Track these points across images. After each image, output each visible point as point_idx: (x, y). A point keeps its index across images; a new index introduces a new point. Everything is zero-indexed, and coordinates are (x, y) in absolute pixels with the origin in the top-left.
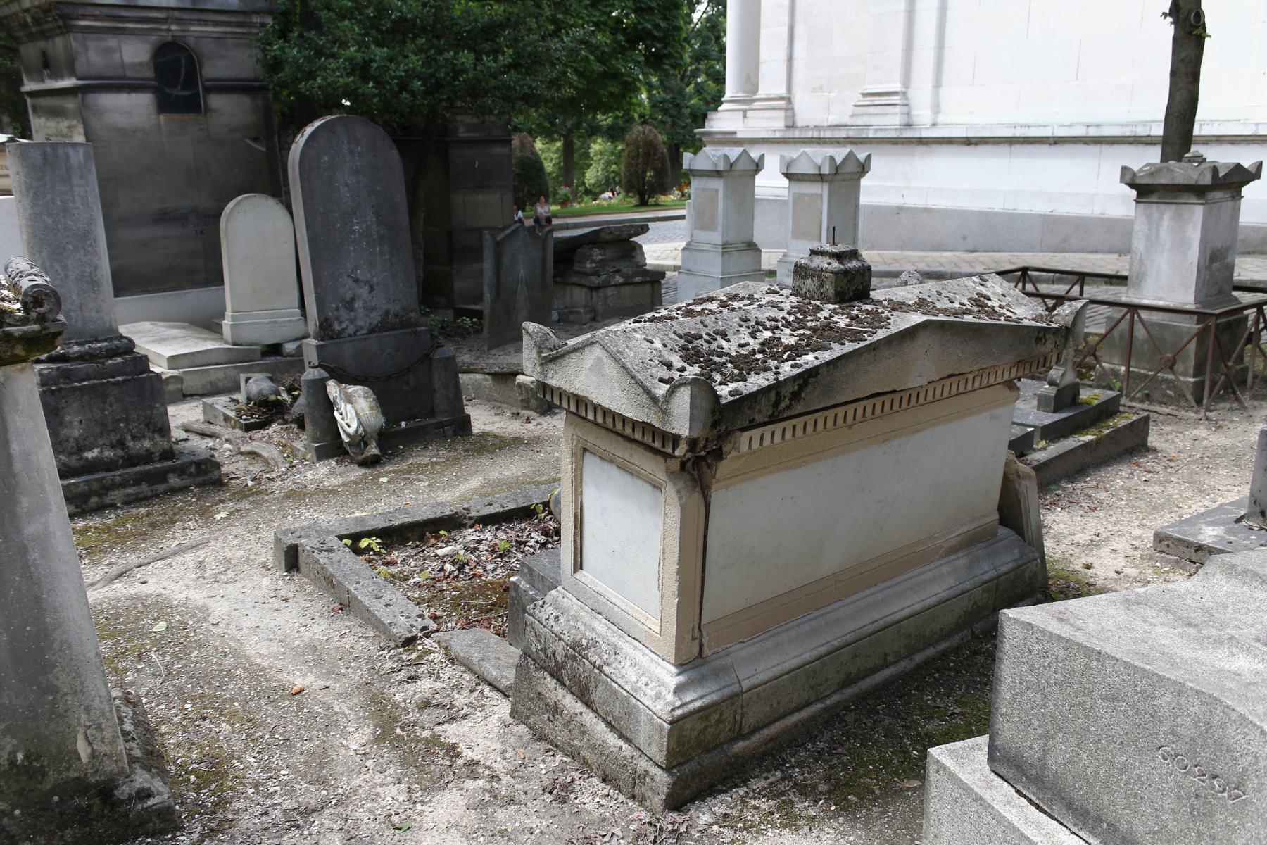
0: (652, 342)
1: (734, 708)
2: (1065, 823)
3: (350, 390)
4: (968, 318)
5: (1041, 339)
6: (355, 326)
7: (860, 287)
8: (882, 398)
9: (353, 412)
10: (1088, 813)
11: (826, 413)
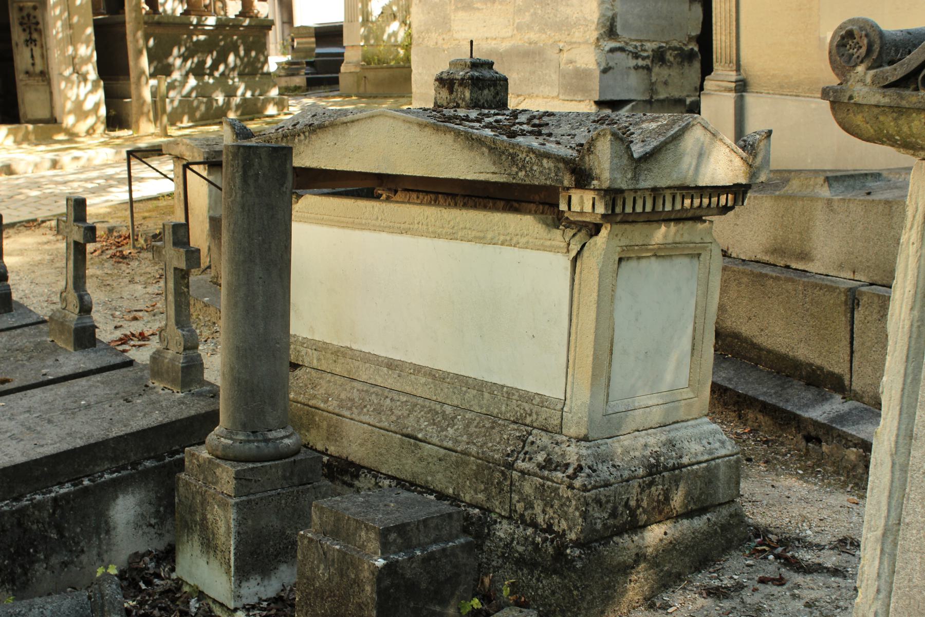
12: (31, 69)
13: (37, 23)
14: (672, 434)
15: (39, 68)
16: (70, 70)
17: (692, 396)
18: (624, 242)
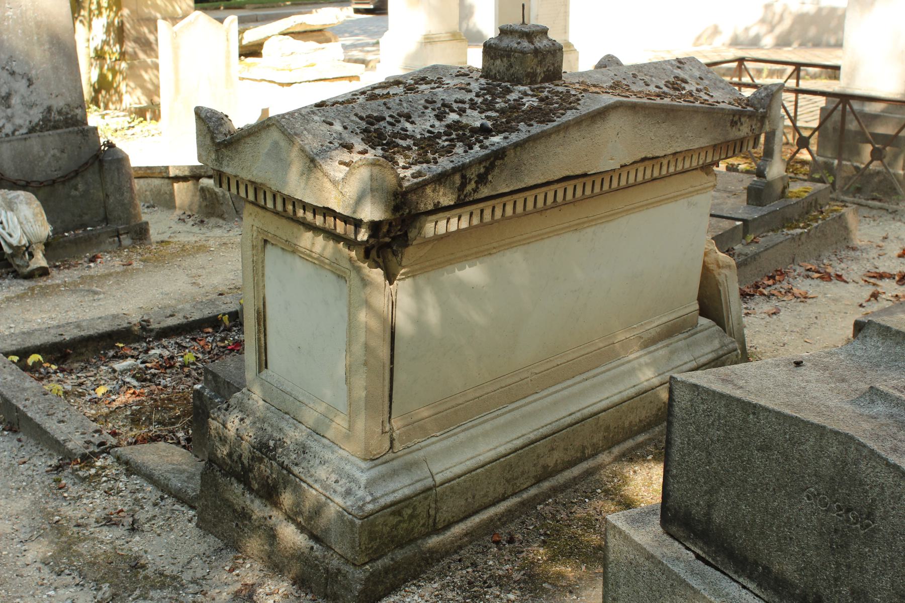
0: (331, 124)
1: (427, 502)
2: (727, 572)
3: (9, 197)
4: (667, 101)
5: (736, 123)
6: (13, 124)
7: (552, 68)
8: (573, 182)
9: (15, 220)
10: (746, 559)
11: (515, 197)
14: (313, 444)
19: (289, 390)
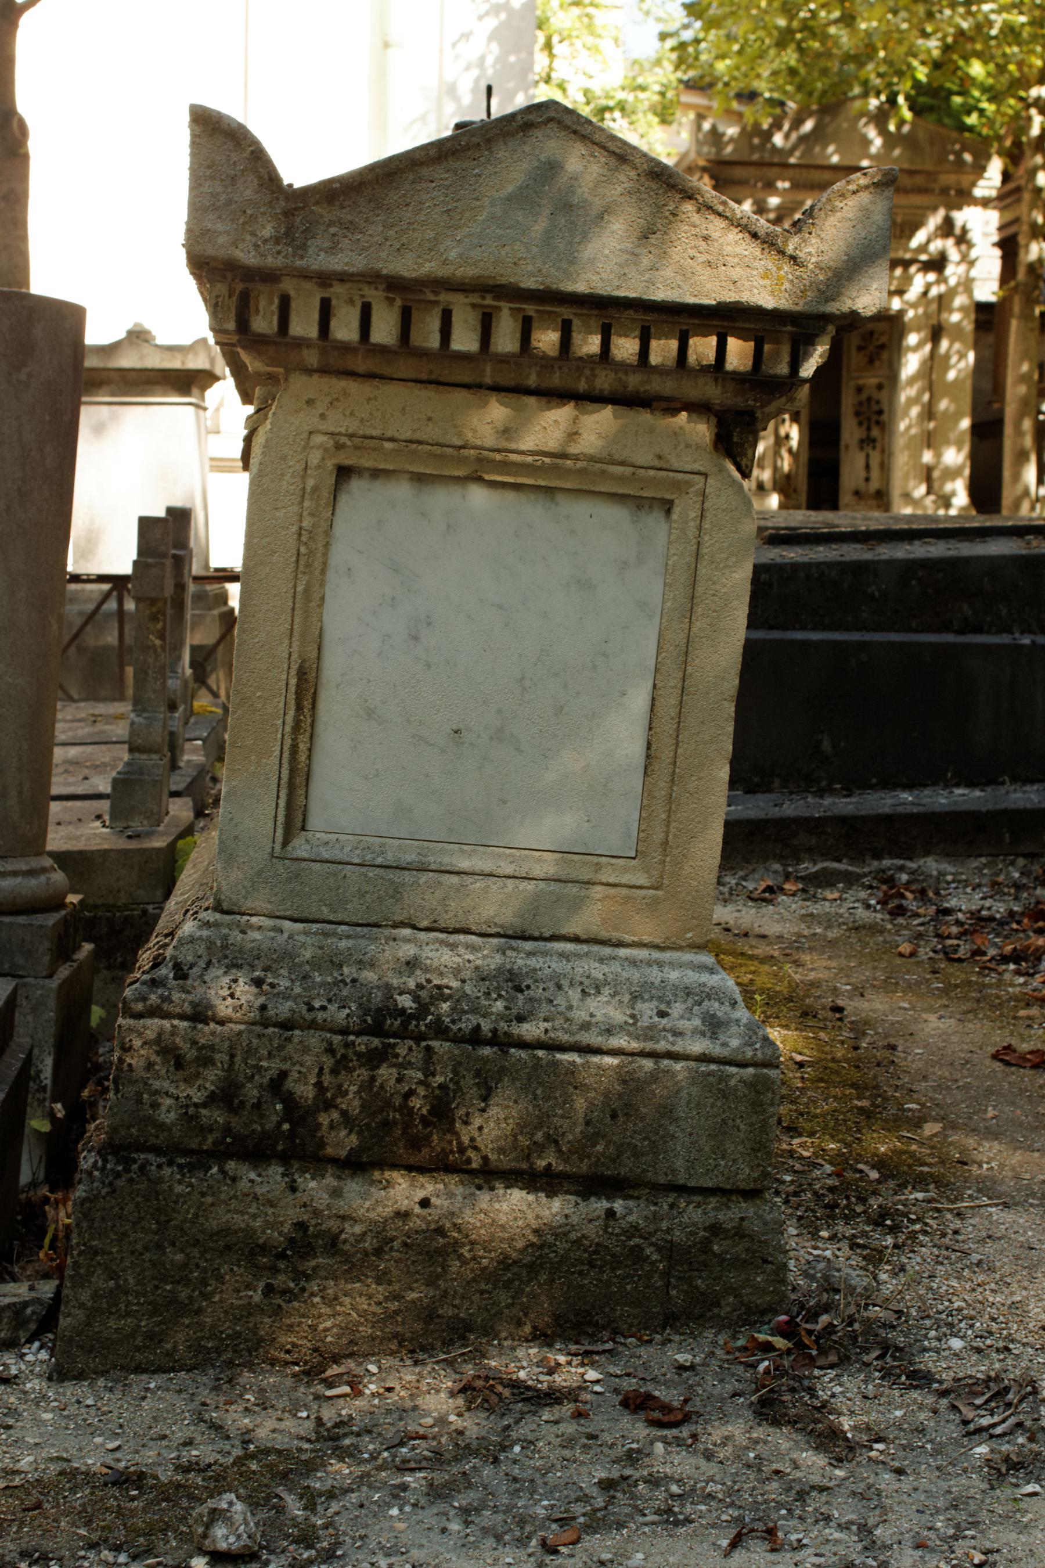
12: (862, 485)
13: (880, 412)
14: (520, 962)
15: (874, 485)
16: (922, 489)
17: (643, 880)
18: (339, 422)
19: (410, 857)
